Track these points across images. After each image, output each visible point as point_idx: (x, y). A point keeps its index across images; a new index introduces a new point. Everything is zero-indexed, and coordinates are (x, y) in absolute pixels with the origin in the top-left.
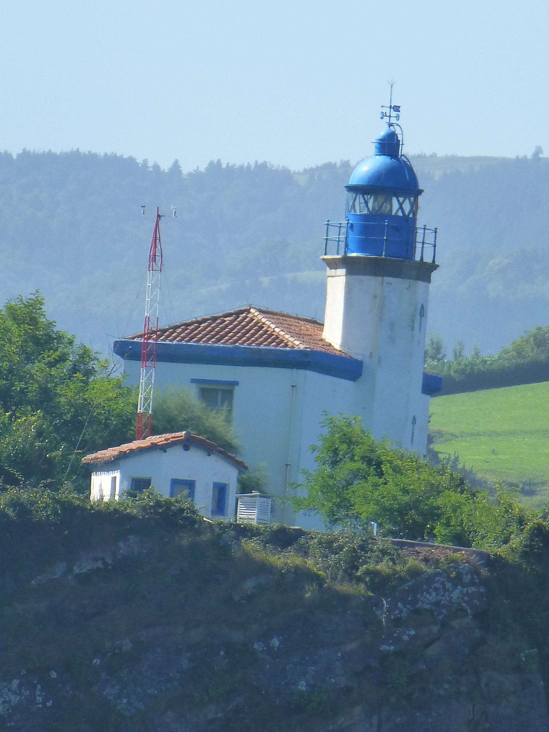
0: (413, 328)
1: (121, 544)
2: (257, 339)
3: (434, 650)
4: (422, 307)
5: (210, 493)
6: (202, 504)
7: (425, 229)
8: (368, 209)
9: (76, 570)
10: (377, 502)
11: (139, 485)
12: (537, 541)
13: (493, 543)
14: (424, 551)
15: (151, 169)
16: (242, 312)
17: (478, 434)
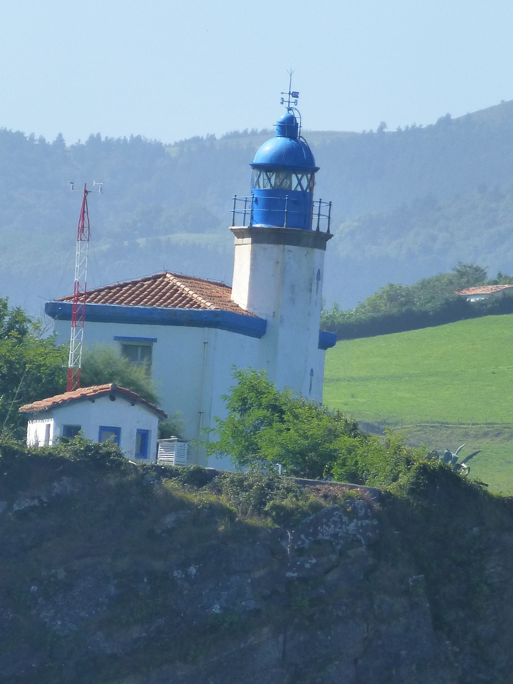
0: (311, 290)
1: (56, 484)
2: (173, 301)
3: (330, 577)
4: (319, 270)
5: (135, 438)
6: (128, 448)
7: (320, 202)
8: (271, 185)
9: (16, 507)
10: (282, 445)
11: (70, 432)
12: (423, 479)
13: (384, 481)
14: (324, 489)
15: (37, 142)
16: (159, 277)
17: (338, 380)
